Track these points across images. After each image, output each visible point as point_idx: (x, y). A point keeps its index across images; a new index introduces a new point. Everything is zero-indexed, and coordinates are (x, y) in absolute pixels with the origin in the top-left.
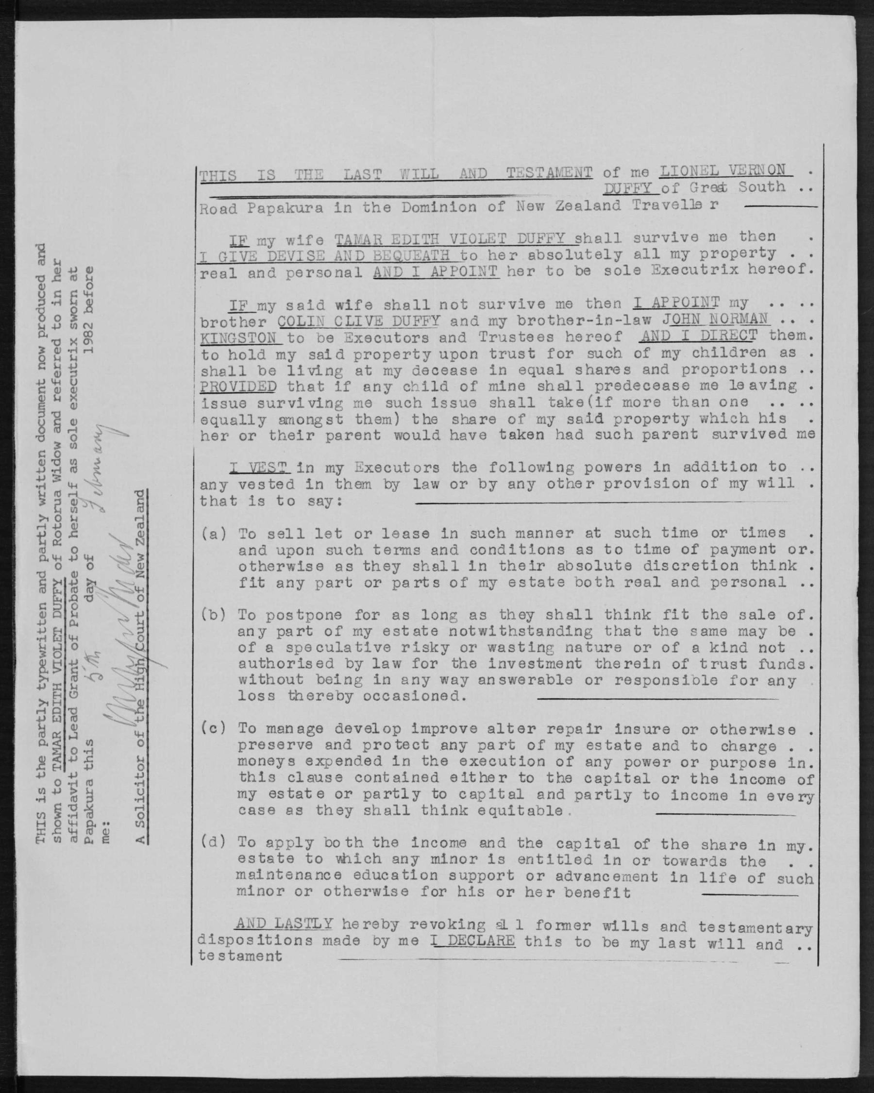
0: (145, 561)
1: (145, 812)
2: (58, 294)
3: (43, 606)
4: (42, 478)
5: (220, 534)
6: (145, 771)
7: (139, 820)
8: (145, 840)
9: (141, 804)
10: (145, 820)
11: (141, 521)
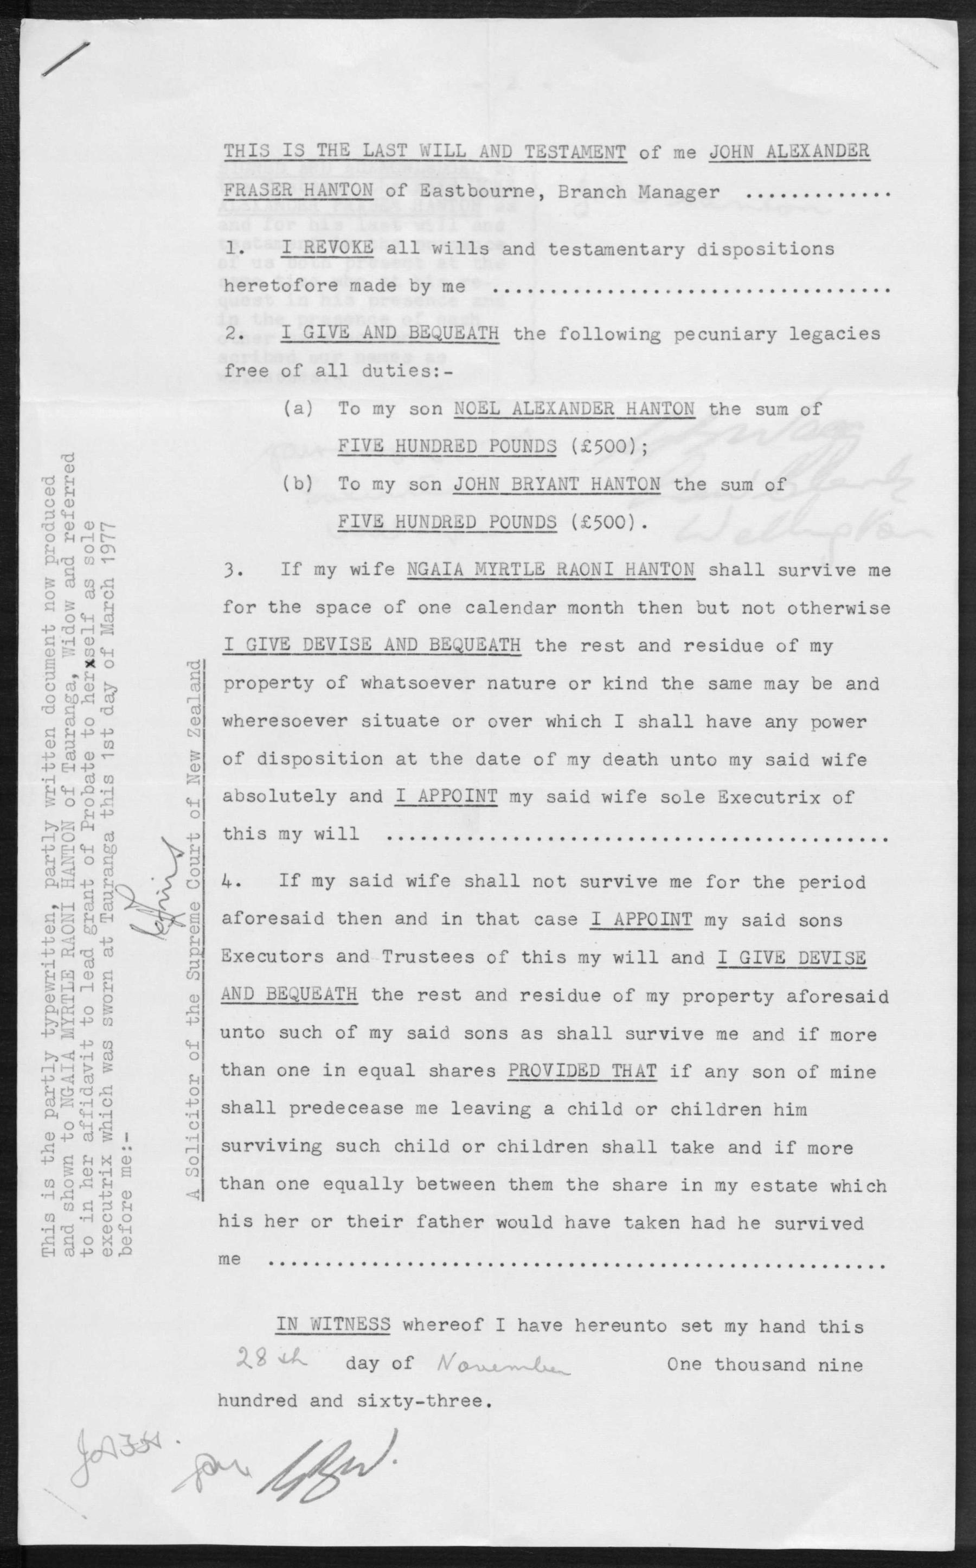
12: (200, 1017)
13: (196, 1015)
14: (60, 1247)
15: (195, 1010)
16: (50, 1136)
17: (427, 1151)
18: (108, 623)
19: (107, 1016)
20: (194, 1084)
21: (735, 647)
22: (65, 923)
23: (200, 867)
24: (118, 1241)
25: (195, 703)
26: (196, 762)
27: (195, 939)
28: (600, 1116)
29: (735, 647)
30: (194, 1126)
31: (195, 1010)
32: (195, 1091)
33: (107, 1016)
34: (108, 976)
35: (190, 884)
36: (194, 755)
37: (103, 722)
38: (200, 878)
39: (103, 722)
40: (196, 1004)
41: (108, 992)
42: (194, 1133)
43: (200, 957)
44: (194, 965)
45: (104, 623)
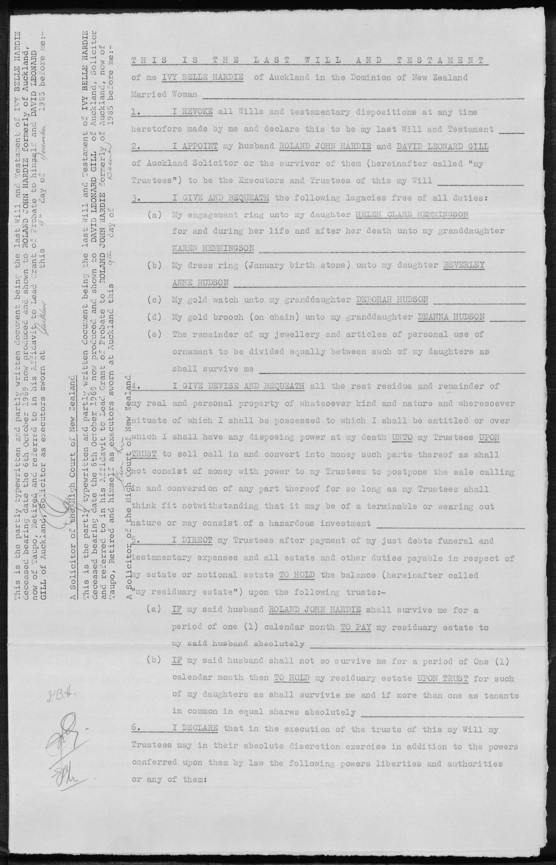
0: (75, 422)
1: (76, 580)
2: (34, 399)
3: (18, 450)
4: (18, 368)
5: (157, 609)
6: (76, 553)
7: (73, 585)
8: (76, 597)
9: (73, 574)
10: (76, 585)
11: (72, 395)
30: (73, 567)
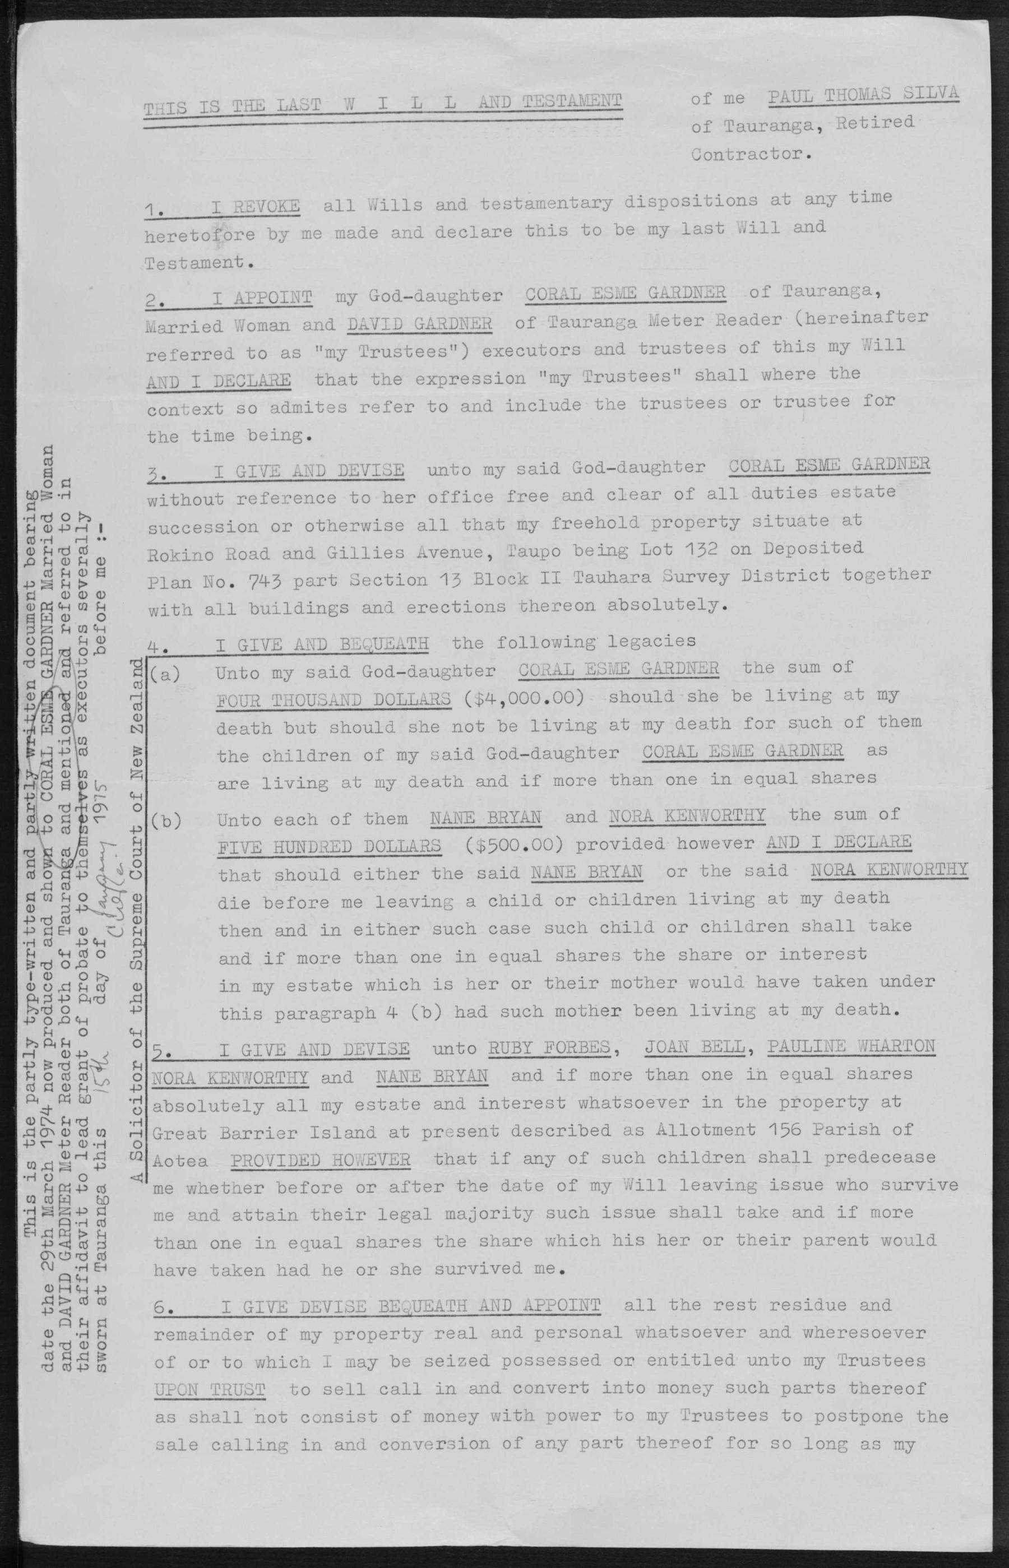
7: (135, 1150)
12: (143, 1005)
13: (139, 1004)
14: (58, 1362)
15: (138, 999)
16: (48, 1288)
17: (449, 502)
18: (48, 578)
19: (101, 1363)
20: (137, 1070)
21: (818, 1306)
22: (62, 1216)
23: (142, 858)
24: (93, 1353)
25: (138, 700)
26: (138, 757)
27: (137, 930)
28: (656, 1192)
29: (818, 1306)
30: (138, 1111)
31: (138, 999)
32: (137, 1077)
33: (101, 1363)
34: (102, 1323)
35: (133, 875)
36: (137, 751)
37: (95, 1179)
38: (142, 869)
39: (95, 1179)
40: (138, 993)
41: (102, 1339)
42: (138, 1118)
43: (143, 947)
44: (138, 954)
45: (44, 579)
